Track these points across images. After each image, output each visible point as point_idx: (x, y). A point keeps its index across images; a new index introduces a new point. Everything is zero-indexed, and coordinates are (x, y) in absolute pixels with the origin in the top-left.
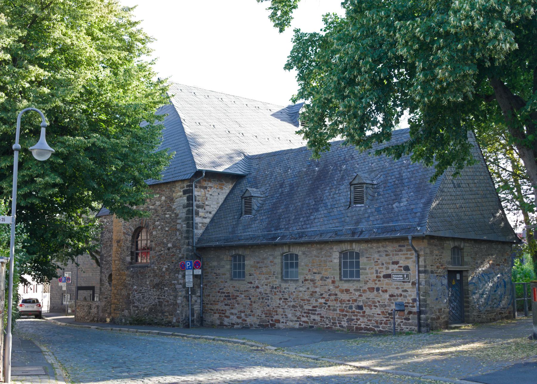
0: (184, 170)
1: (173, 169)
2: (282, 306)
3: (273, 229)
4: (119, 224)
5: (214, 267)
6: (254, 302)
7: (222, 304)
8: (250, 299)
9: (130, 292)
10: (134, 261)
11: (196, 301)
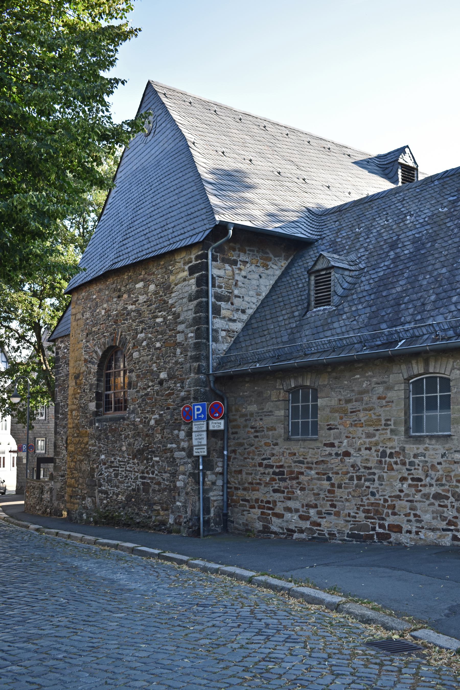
0: (192, 227)
1: (171, 231)
2: (407, 495)
3: (384, 326)
4: (79, 346)
5: (252, 414)
6: (340, 487)
7: (266, 489)
8: (329, 479)
9: (95, 466)
10: (101, 409)
11: (214, 483)
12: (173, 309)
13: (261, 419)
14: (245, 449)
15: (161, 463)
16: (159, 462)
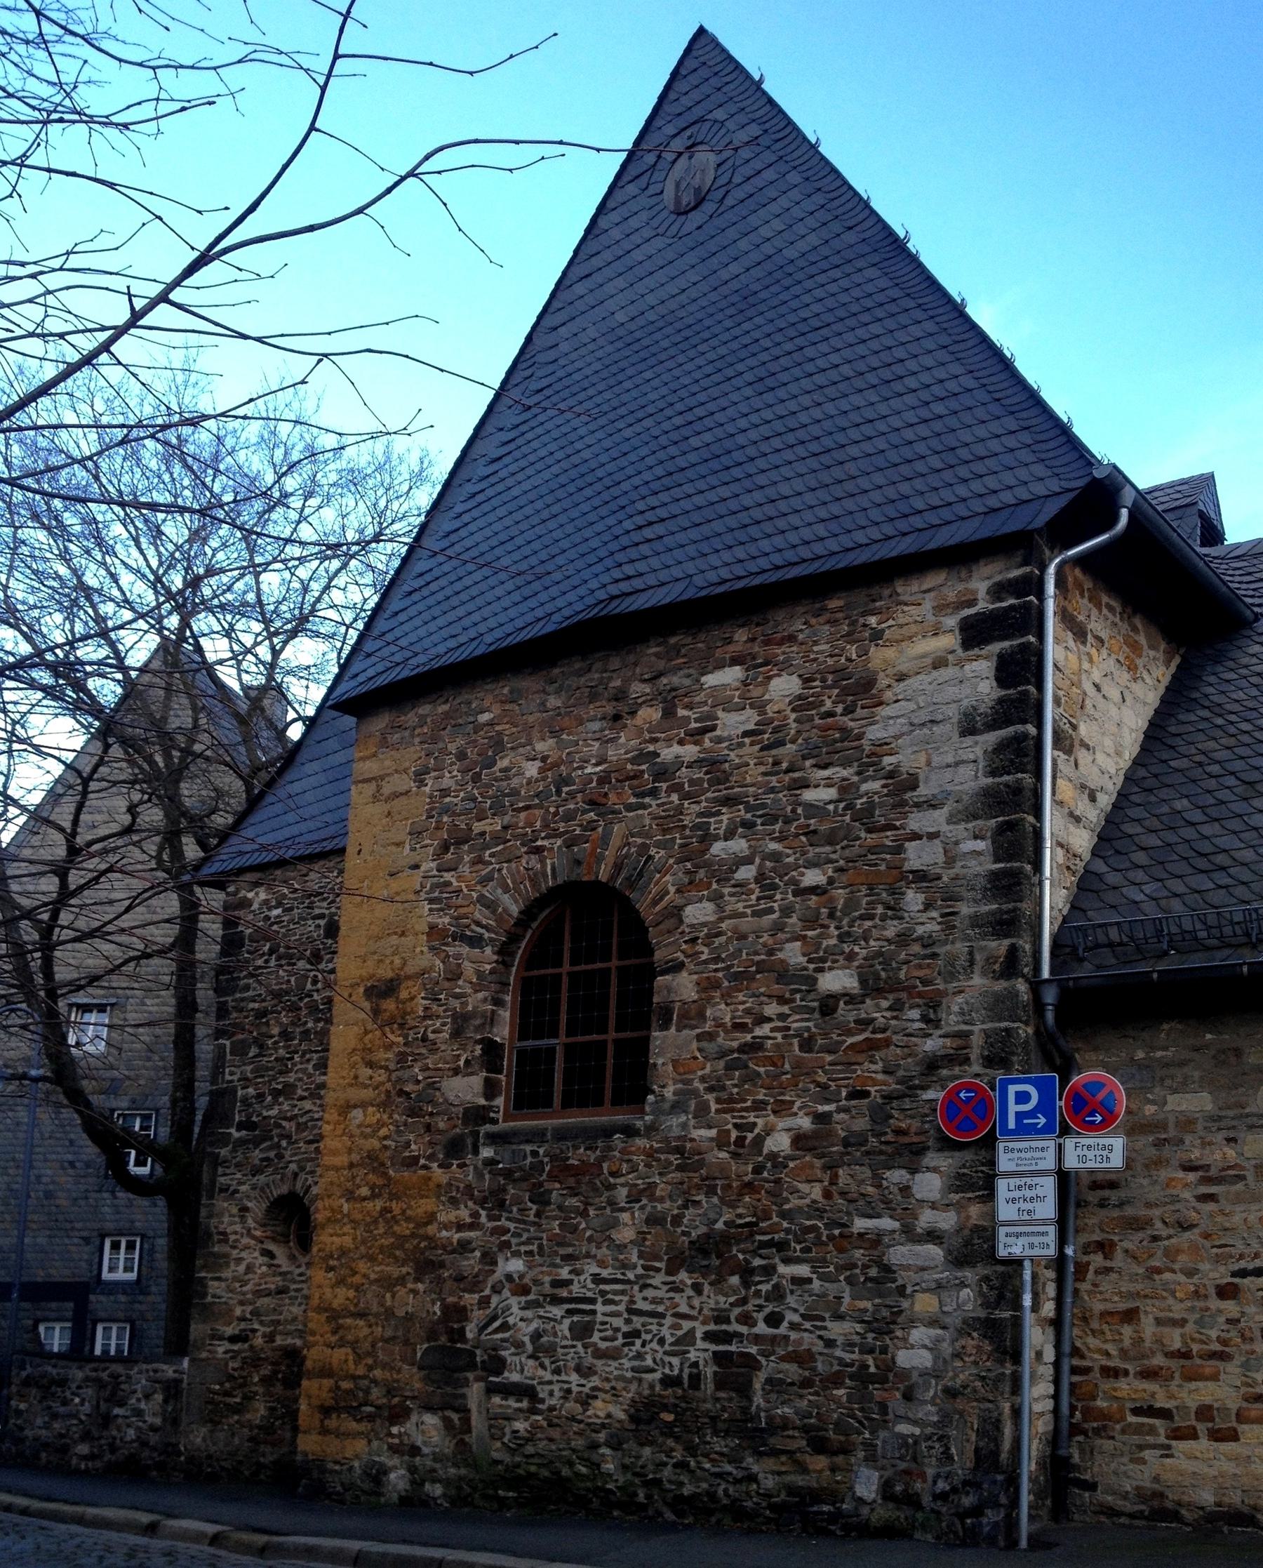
12: (887, 760)
13: (1230, 1140)
14: (1155, 1239)
15: (816, 1284)
16: (810, 1281)
